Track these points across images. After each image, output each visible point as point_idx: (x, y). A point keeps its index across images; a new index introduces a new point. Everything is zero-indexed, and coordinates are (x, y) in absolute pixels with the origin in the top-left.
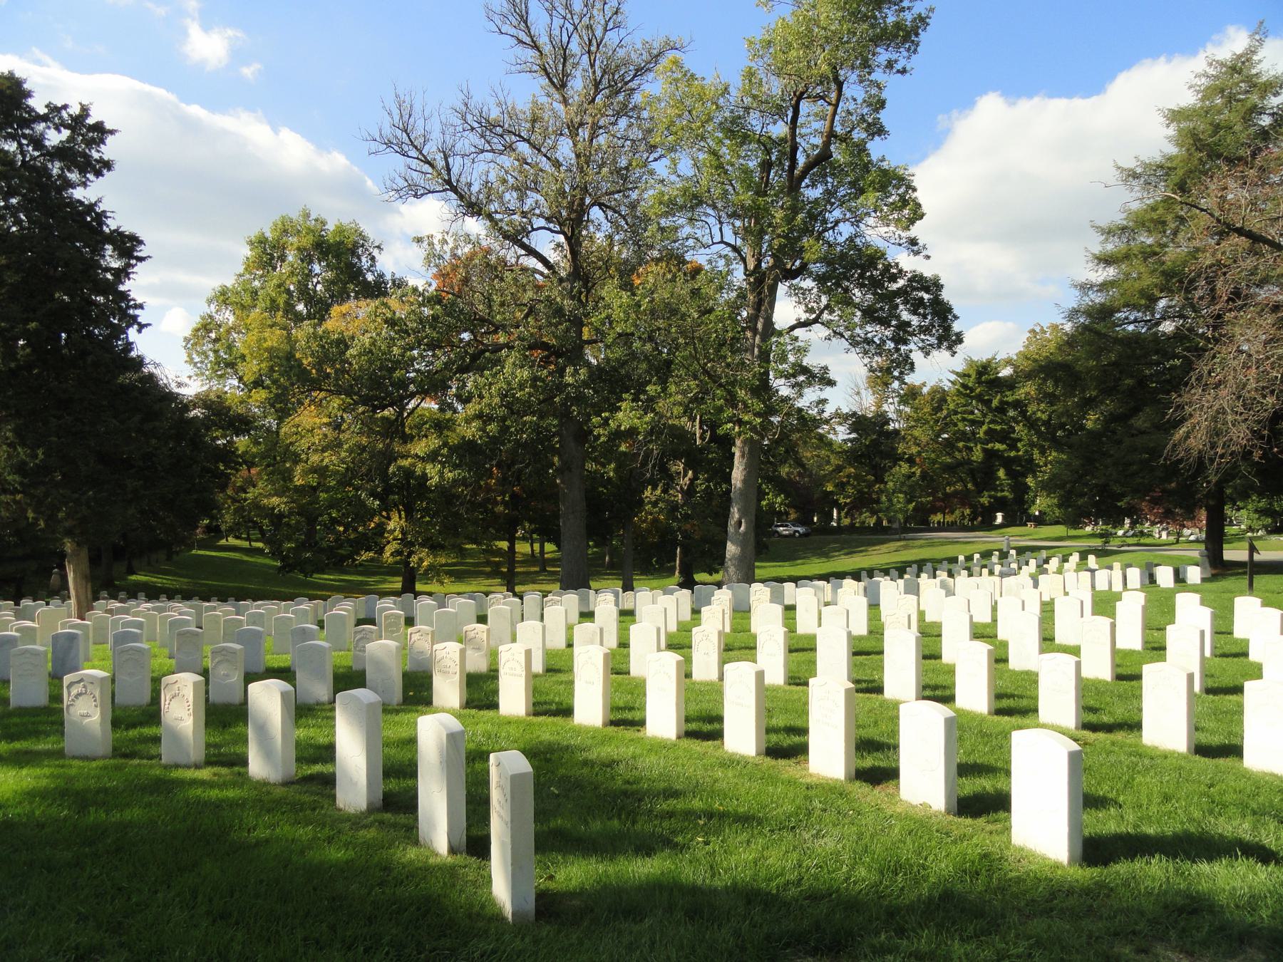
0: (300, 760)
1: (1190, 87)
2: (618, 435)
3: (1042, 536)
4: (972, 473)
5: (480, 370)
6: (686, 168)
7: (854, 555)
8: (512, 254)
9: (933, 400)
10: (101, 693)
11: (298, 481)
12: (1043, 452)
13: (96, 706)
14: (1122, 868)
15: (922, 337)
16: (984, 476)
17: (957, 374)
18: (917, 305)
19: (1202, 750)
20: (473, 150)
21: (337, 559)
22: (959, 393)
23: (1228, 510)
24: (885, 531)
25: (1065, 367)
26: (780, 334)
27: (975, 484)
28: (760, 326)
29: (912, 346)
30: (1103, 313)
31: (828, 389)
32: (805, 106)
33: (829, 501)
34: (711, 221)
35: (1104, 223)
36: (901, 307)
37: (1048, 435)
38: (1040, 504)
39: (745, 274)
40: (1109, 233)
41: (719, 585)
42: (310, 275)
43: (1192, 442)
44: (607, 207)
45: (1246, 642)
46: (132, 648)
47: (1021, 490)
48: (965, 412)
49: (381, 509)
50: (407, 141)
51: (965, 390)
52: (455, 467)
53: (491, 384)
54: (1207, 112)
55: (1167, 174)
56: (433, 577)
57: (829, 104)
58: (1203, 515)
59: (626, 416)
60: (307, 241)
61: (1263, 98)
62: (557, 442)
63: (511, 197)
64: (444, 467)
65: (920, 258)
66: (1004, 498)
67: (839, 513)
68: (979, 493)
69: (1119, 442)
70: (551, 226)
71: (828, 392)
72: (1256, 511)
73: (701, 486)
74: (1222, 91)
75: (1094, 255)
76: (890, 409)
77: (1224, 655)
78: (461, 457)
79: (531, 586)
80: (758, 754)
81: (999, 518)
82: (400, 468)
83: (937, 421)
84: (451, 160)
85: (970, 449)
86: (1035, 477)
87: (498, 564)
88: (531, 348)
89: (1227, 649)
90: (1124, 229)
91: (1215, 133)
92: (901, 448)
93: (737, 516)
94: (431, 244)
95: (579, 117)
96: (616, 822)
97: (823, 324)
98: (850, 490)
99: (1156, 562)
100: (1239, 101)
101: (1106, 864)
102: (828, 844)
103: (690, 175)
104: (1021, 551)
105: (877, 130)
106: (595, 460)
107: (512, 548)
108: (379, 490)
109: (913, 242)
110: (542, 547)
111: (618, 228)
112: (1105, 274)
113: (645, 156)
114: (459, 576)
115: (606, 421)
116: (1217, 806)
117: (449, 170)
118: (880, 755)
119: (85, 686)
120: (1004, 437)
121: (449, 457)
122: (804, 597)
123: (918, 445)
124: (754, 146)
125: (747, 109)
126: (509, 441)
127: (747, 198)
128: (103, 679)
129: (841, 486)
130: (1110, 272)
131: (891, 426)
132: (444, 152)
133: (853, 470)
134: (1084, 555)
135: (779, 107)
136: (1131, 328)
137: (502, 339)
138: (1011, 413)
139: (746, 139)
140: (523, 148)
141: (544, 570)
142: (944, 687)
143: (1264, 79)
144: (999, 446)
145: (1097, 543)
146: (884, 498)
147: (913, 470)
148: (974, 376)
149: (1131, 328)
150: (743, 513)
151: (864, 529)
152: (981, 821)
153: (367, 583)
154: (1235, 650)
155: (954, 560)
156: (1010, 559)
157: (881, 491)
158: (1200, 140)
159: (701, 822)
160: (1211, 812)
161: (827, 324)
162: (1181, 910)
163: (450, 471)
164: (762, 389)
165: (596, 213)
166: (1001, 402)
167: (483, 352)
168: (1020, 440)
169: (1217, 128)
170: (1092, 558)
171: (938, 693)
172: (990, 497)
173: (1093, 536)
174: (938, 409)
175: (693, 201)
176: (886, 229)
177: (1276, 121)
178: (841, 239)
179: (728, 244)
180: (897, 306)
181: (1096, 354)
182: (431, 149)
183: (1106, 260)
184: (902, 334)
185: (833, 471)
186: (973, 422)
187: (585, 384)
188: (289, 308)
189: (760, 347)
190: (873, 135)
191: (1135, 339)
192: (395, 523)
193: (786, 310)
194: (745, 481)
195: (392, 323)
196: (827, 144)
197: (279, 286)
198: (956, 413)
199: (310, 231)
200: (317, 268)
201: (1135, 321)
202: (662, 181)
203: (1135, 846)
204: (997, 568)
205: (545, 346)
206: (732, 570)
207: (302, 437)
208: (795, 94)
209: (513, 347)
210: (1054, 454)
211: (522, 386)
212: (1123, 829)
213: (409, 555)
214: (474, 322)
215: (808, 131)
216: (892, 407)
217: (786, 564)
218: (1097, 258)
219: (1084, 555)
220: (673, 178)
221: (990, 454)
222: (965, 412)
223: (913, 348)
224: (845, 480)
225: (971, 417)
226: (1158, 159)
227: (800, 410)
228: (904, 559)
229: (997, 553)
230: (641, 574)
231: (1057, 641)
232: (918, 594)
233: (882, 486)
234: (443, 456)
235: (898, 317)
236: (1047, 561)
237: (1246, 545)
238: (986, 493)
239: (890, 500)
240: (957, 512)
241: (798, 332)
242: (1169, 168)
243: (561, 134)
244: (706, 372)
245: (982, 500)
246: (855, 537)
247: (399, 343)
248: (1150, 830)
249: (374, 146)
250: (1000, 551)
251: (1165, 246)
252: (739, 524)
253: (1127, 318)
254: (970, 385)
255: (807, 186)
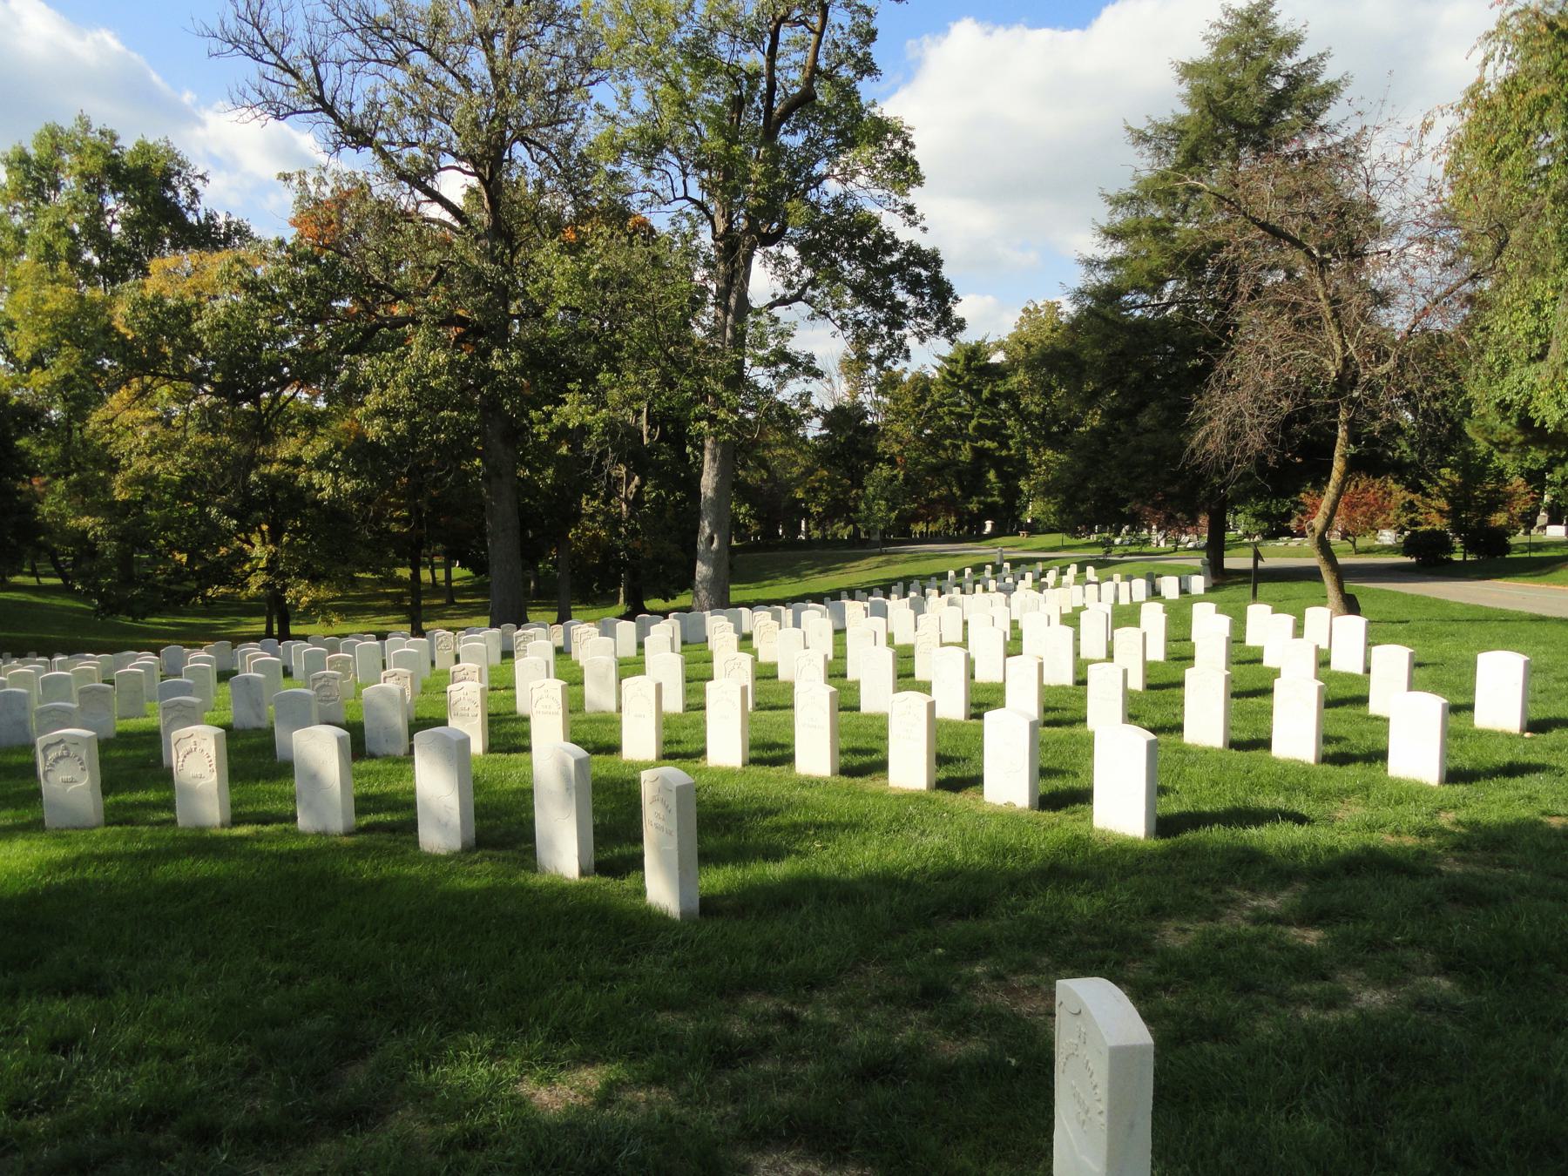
0: (360, 812)
1: (1204, 39)
2: (562, 433)
3: (1035, 547)
4: (959, 476)
5: (375, 351)
6: (641, 103)
7: (831, 573)
8: (406, 197)
9: (915, 389)
10: (89, 753)
11: (120, 495)
12: (1036, 452)
13: (83, 770)
14: (1189, 836)
15: (919, 320)
16: (972, 479)
17: (943, 359)
18: (914, 285)
19: (1234, 745)
20: (349, 55)
21: (173, 597)
22: (945, 382)
23: (1230, 518)
24: (864, 544)
25: (1069, 356)
26: (759, 313)
27: (962, 488)
28: (732, 302)
29: (906, 331)
30: (1109, 296)
31: (815, 382)
32: (785, 33)
33: (797, 511)
34: (675, 172)
35: (1113, 192)
36: (897, 284)
37: (1053, 431)
38: (1033, 511)
39: (713, 238)
40: (1117, 203)
41: (665, 615)
42: (100, 213)
43: (1210, 446)
44: (531, 142)
45: (1260, 650)
46: (179, 703)
47: (1012, 493)
48: (953, 404)
49: (240, 528)
50: (260, 39)
51: (952, 378)
52: (356, 475)
53: (394, 371)
54: (1221, 69)
55: (1178, 138)
56: (317, 616)
57: (812, 31)
58: (1203, 520)
59: (573, 410)
60: (95, 164)
61: (1277, 56)
62: (477, 443)
63: (409, 125)
64: (337, 476)
65: (916, 229)
66: (995, 503)
67: (807, 524)
68: (967, 498)
69: (1125, 442)
70: (463, 165)
71: (815, 386)
72: (1254, 515)
73: (650, 493)
74: (1238, 45)
75: (1102, 228)
76: (867, 399)
77: (1240, 662)
78: (357, 463)
79: (438, 623)
80: (833, 774)
81: (989, 525)
82: (262, 477)
83: (920, 414)
84: (322, 69)
85: (958, 447)
86: (1028, 479)
87: (399, 597)
88: (442, 324)
89: (1243, 656)
90: (1132, 198)
91: (1229, 94)
92: (881, 446)
93: (708, 531)
94: (303, 183)
95: (495, 22)
96: (729, 838)
97: (806, 301)
98: (823, 497)
99: (1156, 572)
100: (1253, 59)
101: (1176, 835)
102: (937, 840)
103: (645, 111)
104: (1015, 564)
105: (866, 67)
106: (529, 465)
107: (416, 576)
108: (236, 505)
109: (910, 210)
110: (448, 574)
111: (550, 174)
112: (1113, 250)
113: (579, 78)
114: (350, 611)
115: (549, 415)
116: (1256, 786)
117: (320, 83)
118: (951, 767)
119: (66, 748)
120: (995, 433)
121: (344, 462)
122: (759, 621)
123: (900, 443)
124: (721, 77)
125: (714, 31)
126: (423, 443)
127: (717, 144)
128: (90, 738)
129: (813, 492)
130: (1119, 249)
131: (869, 420)
132: (312, 58)
133: (826, 473)
134: (1082, 568)
135: (753, 32)
136: (1138, 313)
137: (398, 310)
138: (1003, 406)
139: (711, 68)
140: (420, 59)
141: (453, 602)
142: (783, 746)
143: (1280, 35)
144: (989, 444)
145: (1098, 552)
146: (862, 506)
147: (895, 472)
148: (962, 362)
149: (1138, 313)
150: (716, 526)
151: (837, 543)
152: (1061, 814)
153: (214, 627)
154: (1250, 657)
155: (943, 576)
156: (1004, 573)
157: (858, 498)
158: (1214, 101)
159: (811, 833)
160: (1252, 791)
161: (810, 302)
162: (1241, 861)
163: (347, 481)
164: (737, 381)
165: (519, 150)
166: (993, 393)
167: (377, 327)
168: (1012, 437)
169: (1231, 88)
170: (1090, 570)
171: (771, 754)
172: (979, 502)
173: (1095, 544)
174: (922, 400)
175: (651, 147)
176: (880, 192)
177: (1290, 84)
178: (825, 200)
179: (693, 201)
180: (891, 284)
181: (1101, 344)
182: (292, 53)
183: (1115, 234)
184: (896, 319)
185: (803, 474)
186: (961, 416)
187: (520, 371)
188: (74, 256)
189: (734, 330)
190: (863, 73)
191: (1141, 327)
192: (259, 551)
193: (762, 282)
194: (717, 490)
195: (251, 286)
196: (809, 81)
197: (58, 225)
198: (941, 405)
199: (97, 149)
200: (110, 203)
201: (1143, 305)
202: (613, 119)
203: (1196, 820)
204: (992, 585)
205: (462, 322)
206: (703, 594)
207: (119, 436)
208: (774, 18)
209: (420, 322)
210: (1049, 452)
211: (436, 373)
212: (1183, 809)
213: (284, 589)
214: (363, 287)
215: (787, 63)
216: (869, 398)
217: (752, 586)
218: (1105, 232)
219: (1082, 568)
220: (625, 115)
221: (980, 454)
222: (953, 404)
223: (908, 332)
224: (817, 485)
225: (959, 410)
226: (1170, 121)
227: (782, 405)
228: (887, 576)
229: (989, 567)
230: (581, 604)
231: (918, 677)
232: (886, 617)
233: (860, 492)
234: (335, 461)
235: (892, 296)
236: (1043, 574)
237: (1250, 551)
238: (975, 499)
239: (869, 508)
240: (941, 520)
241: (779, 311)
242: (1182, 132)
243: (471, 43)
244: (669, 357)
245: (970, 506)
246: (828, 552)
247: (263, 314)
248: (1207, 809)
249: (216, 45)
250: (992, 564)
251: (1175, 221)
252: (711, 539)
253: (1134, 302)
254: (958, 372)
255: (786, 132)
